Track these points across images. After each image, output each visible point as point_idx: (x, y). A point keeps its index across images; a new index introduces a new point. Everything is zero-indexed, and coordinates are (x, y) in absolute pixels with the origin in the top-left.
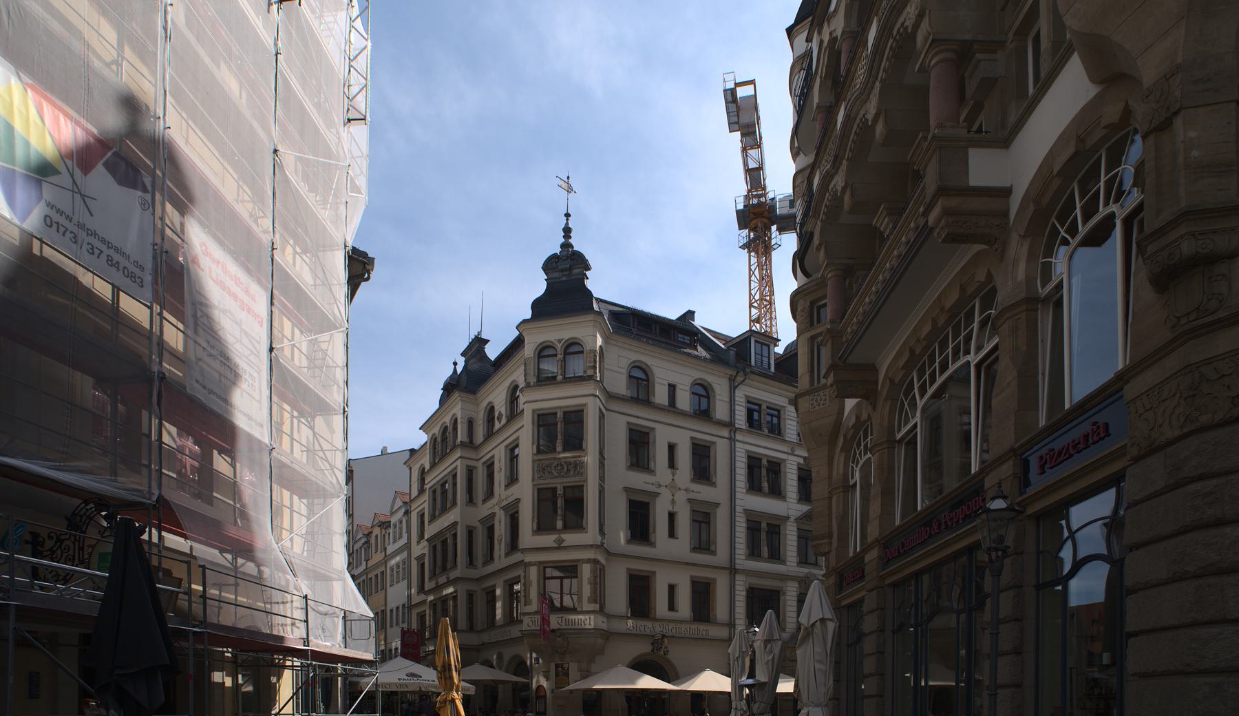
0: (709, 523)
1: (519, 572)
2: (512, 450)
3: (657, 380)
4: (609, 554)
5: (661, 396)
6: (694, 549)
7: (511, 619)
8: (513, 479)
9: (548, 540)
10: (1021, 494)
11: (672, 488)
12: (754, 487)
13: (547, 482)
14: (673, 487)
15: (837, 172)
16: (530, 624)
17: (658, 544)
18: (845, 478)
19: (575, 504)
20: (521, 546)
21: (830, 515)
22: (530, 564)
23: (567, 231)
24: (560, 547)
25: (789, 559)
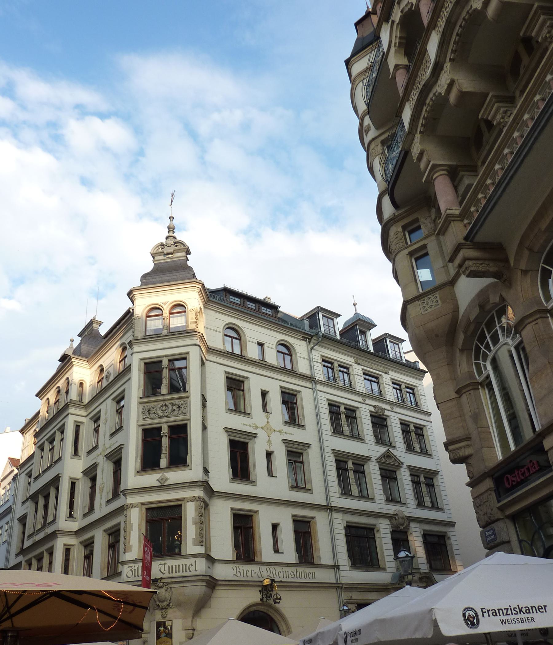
2: (118, 402)
3: (248, 339)
6: (295, 487)
9: (151, 479)
11: (269, 431)
13: (152, 422)
14: (267, 428)
17: (259, 482)
22: (132, 506)
24: (163, 487)
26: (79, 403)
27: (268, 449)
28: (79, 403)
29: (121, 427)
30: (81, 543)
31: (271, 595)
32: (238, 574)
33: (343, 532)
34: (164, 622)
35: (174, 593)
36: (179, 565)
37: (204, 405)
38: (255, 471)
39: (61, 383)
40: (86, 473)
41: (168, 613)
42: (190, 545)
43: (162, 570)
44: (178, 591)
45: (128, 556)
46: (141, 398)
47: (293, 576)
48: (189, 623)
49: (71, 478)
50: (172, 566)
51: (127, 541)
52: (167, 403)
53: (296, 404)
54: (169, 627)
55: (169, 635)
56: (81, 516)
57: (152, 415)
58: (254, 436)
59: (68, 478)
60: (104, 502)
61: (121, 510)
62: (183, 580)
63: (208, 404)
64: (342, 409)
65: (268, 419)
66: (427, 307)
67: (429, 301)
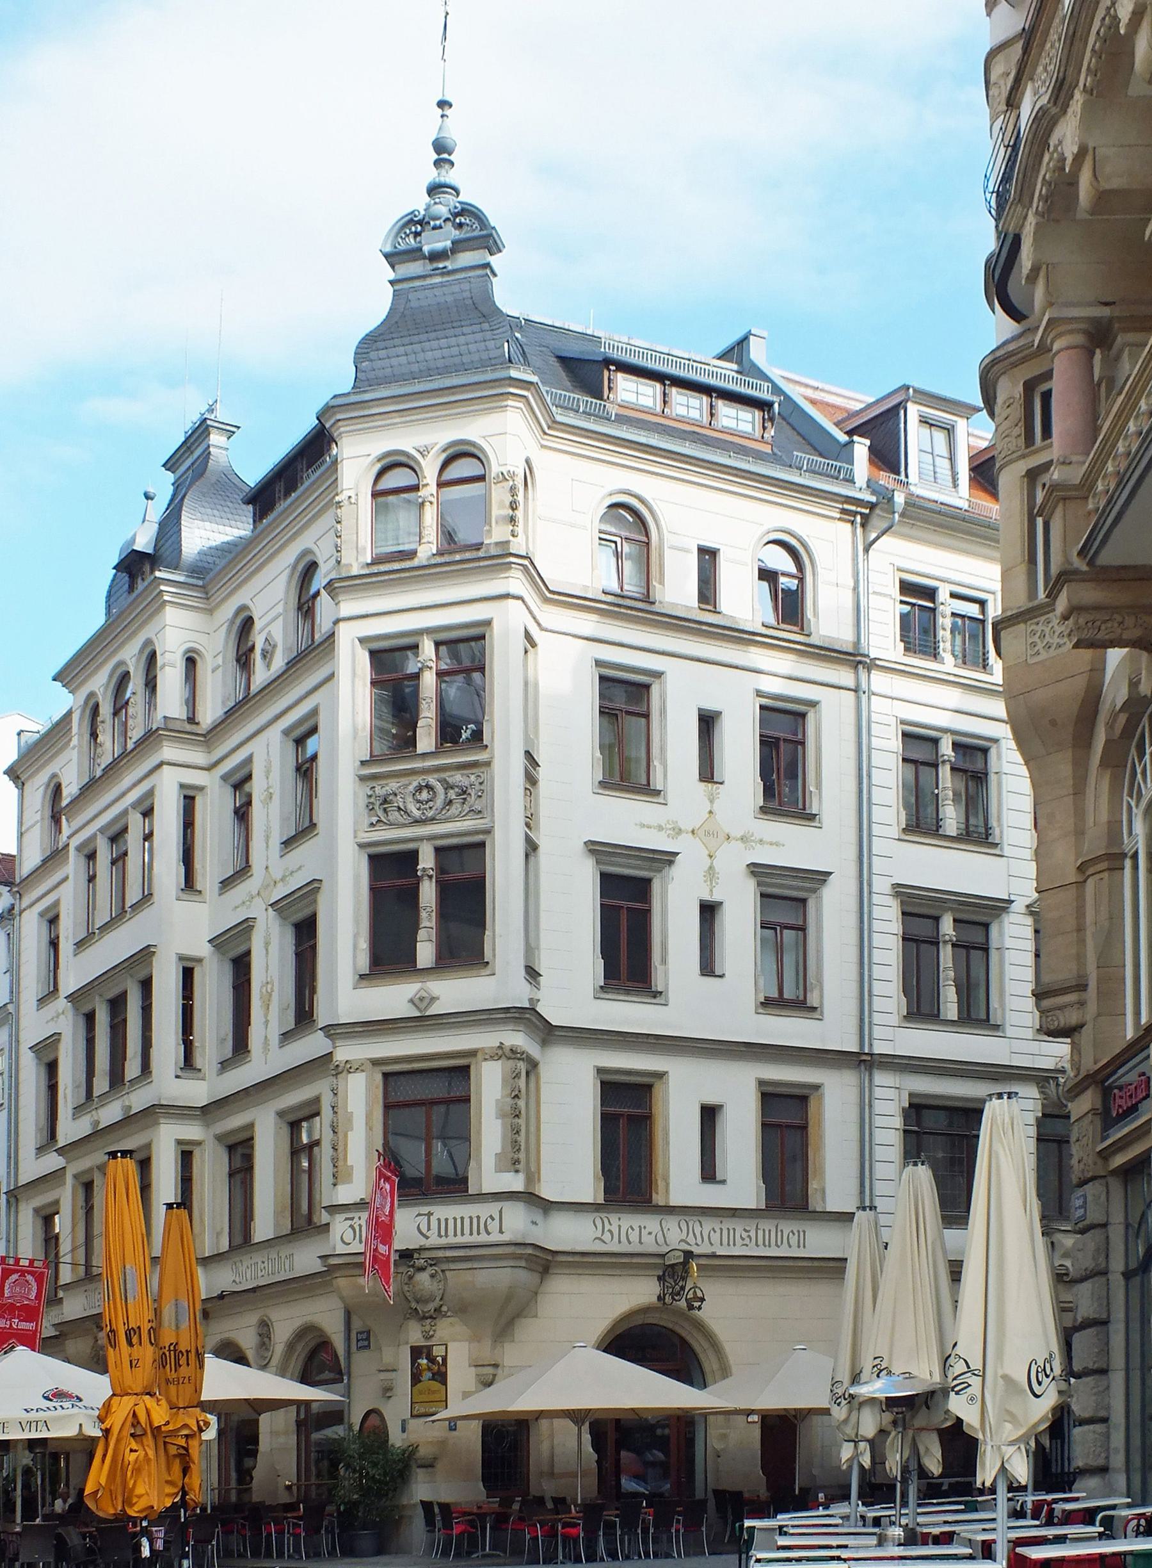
0: (803, 929)
1: (319, 1088)
2: (300, 742)
4: (548, 1033)
5: (678, 589)
6: (773, 1004)
7: (304, 1223)
8: (304, 830)
9: (393, 998)
10: (1104, 1139)
12: (921, 823)
14: (710, 833)
15: (1064, 111)
16: (346, 1236)
18: (1114, 832)
19: (466, 898)
20: (323, 1017)
21: (1080, 929)
22: (350, 1068)
23: (442, 150)
24: (423, 1021)
25: (1011, 1018)
26: (189, 727)
27: (707, 897)
28: (189, 727)
29: (313, 826)
30: (219, 1138)
31: (683, 1288)
32: (607, 1237)
33: (898, 1122)
34: (429, 1348)
35: (450, 1283)
36: (462, 1218)
37: (531, 780)
38: (664, 961)
39: (130, 655)
40: (218, 942)
41: (437, 1328)
42: (489, 1174)
43: (424, 1229)
44: (459, 1279)
45: (346, 1194)
46: (363, 763)
47: (747, 1241)
48: (486, 1352)
49: (181, 958)
50: (447, 1220)
51: (341, 1156)
52: (432, 780)
53: (803, 743)
54: (439, 1359)
55: (441, 1377)
56: (216, 1067)
57: (394, 816)
58: (667, 859)
59: (174, 959)
60: (275, 1039)
61: (322, 1064)
62: (471, 1255)
63: (542, 774)
64: (946, 748)
65: (712, 802)
66: (1040, 646)
67: (1047, 630)
